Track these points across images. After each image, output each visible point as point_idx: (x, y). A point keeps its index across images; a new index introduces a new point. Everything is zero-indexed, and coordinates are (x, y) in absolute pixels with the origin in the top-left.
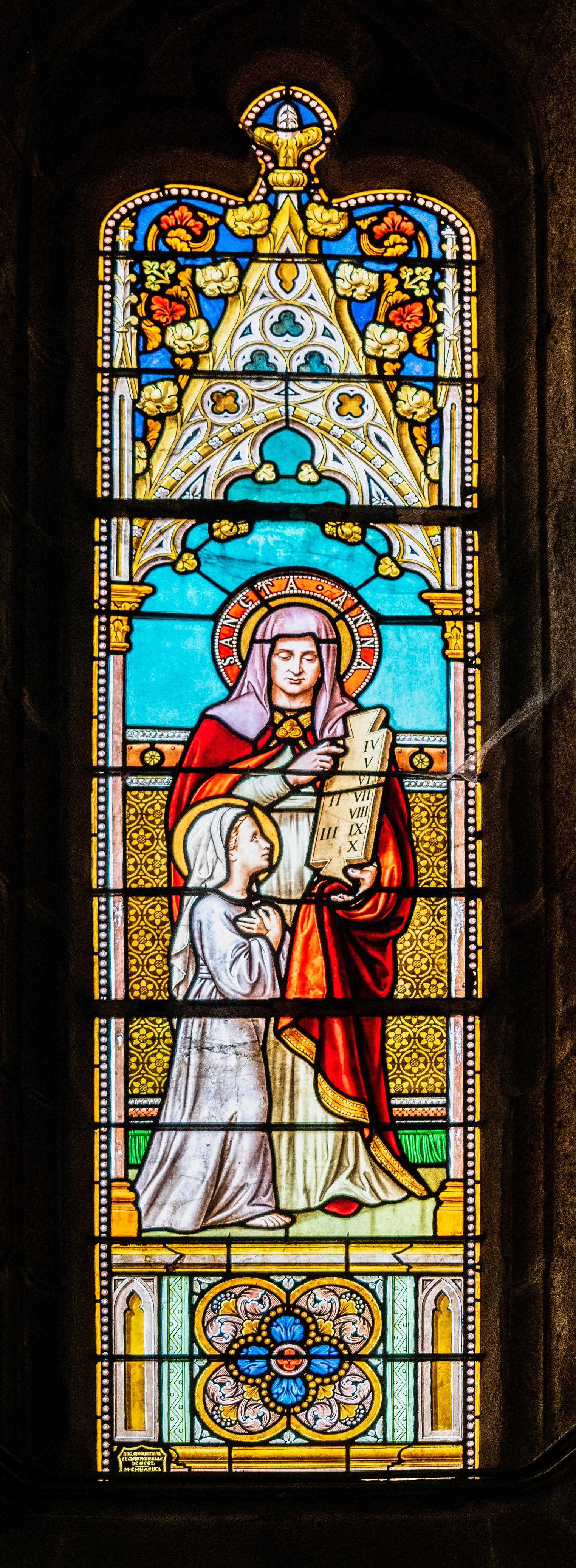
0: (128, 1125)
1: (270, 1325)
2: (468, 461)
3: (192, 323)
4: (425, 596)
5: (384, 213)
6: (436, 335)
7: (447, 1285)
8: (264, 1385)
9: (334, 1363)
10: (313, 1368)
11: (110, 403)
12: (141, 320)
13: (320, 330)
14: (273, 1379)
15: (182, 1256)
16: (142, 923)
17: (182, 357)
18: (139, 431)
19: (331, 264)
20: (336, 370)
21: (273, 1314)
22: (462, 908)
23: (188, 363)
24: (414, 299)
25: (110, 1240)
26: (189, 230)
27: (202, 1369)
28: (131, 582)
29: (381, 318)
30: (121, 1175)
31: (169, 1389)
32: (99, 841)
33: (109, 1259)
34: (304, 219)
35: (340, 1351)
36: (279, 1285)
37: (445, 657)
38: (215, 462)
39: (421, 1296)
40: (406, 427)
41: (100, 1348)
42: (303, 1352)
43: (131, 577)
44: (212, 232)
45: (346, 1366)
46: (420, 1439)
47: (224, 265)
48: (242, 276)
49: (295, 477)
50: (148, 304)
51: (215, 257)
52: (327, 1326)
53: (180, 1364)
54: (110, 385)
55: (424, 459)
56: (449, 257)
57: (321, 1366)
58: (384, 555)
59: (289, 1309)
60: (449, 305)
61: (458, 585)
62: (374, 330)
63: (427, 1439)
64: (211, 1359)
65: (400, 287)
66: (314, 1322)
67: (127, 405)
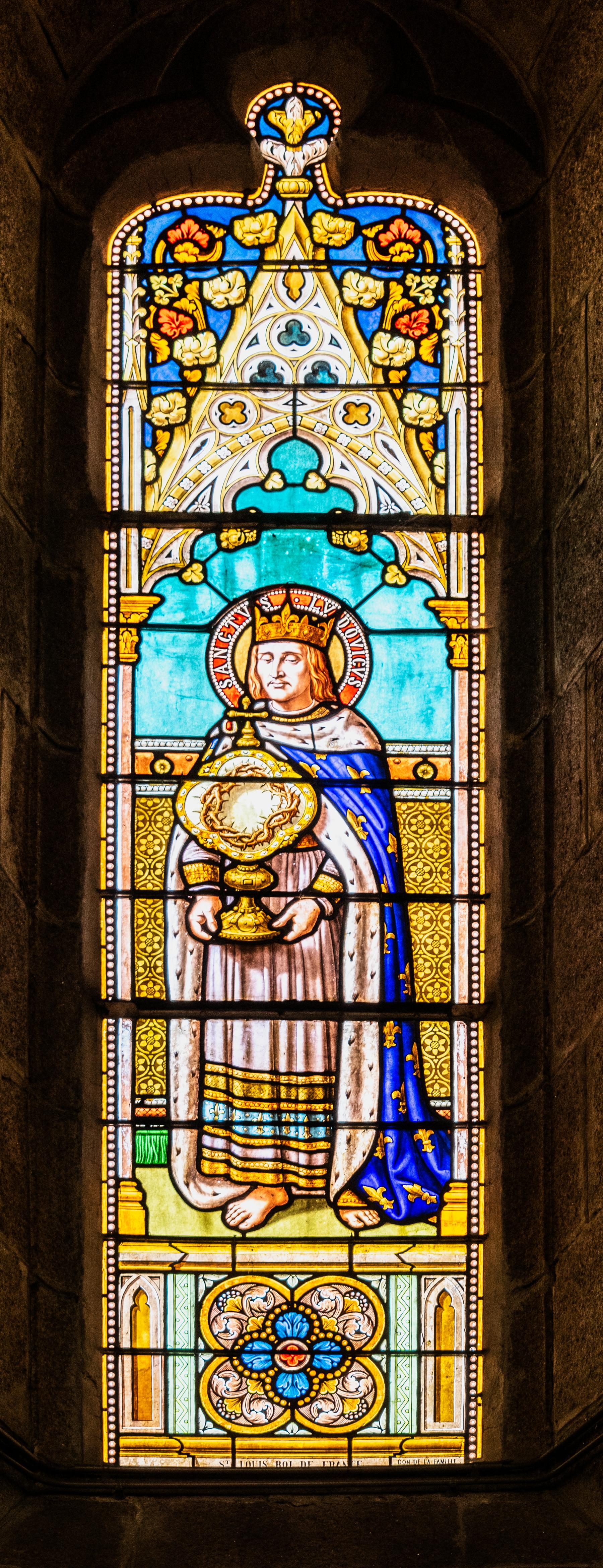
0: (135, 1122)
1: (274, 1322)
2: (474, 464)
3: (200, 336)
4: (432, 604)
5: (391, 220)
6: (441, 341)
7: (449, 1283)
8: (268, 1380)
9: (337, 1359)
10: (316, 1364)
11: (119, 413)
12: (150, 332)
13: (328, 339)
14: (277, 1374)
15: (186, 1254)
16: (150, 926)
17: (192, 368)
18: (149, 439)
19: (338, 270)
20: (342, 381)
21: (277, 1311)
22: (466, 912)
23: (194, 376)
24: (418, 307)
25: (119, 1238)
26: (196, 244)
27: (208, 1363)
28: (140, 593)
29: (387, 326)
30: (128, 1175)
31: (175, 1406)
32: (108, 844)
33: (116, 1256)
34: (310, 227)
35: (343, 1348)
36: (284, 1283)
37: (449, 666)
38: (221, 474)
39: (424, 1295)
40: (412, 433)
41: (106, 1341)
42: (305, 1348)
43: (140, 588)
44: (219, 245)
45: (348, 1363)
46: (423, 1431)
47: (230, 276)
48: (249, 284)
49: (303, 485)
50: (157, 316)
51: (222, 266)
52: (329, 1322)
53: (186, 1358)
54: (120, 396)
55: (431, 466)
56: (454, 262)
57: (327, 1362)
58: (391, 563)
59: (293, 1405)
60: (455, 311)
61: (464, 594)
62: (382, 338)
63: (429, 1430)
64: (217, 1353)
65: (405, 295)
66: (319, 1319)
67: (137, 415)
